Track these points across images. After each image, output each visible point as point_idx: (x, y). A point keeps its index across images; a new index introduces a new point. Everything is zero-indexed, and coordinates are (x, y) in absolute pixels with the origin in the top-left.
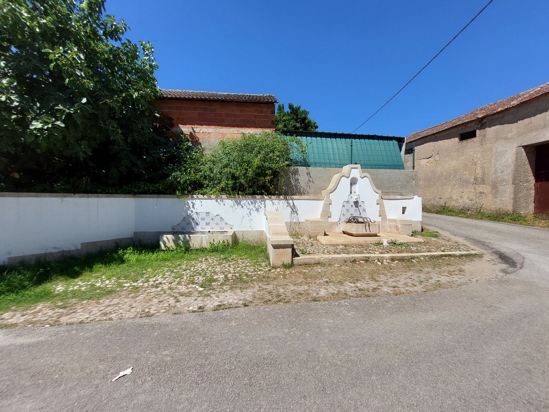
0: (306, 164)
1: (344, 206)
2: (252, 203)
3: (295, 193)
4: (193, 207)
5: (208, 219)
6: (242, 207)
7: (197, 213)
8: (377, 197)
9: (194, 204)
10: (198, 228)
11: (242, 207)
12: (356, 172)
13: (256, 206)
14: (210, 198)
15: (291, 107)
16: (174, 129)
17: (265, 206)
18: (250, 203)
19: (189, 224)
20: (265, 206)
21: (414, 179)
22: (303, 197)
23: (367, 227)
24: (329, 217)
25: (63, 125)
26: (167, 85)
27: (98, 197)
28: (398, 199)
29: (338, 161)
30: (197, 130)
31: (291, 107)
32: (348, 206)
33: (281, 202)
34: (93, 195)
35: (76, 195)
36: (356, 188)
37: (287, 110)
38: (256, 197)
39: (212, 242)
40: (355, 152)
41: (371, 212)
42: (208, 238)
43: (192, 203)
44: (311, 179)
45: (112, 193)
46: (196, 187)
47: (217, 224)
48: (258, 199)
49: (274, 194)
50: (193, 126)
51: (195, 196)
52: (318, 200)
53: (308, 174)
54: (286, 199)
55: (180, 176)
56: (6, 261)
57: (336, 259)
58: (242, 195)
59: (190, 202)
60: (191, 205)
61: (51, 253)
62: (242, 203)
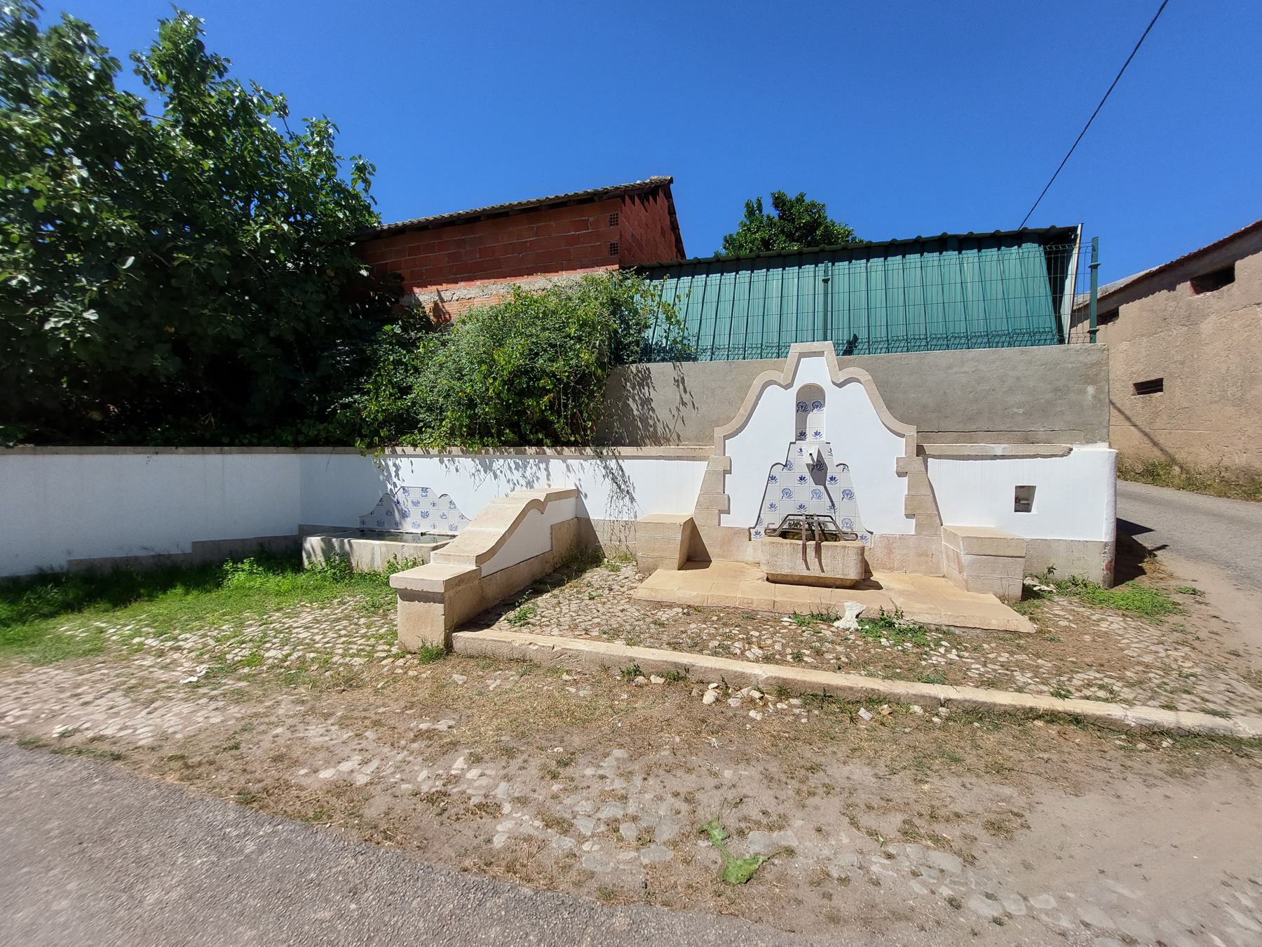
0: (679, 354)
1: (772, 478)
2: (517, 468)
3: (642, 438)
4: (397, 475)
5: (425, 505)
6: (496, 476)
7: (403, 488)
8: (900, 448)
9: (397, 468)
10: (407, 527)
11: (496, 476)
12: (817, 368)
13: (528, 474)
14: (427, 454)
15: (779, 202)
16: (405, 300)
17: (548, 475)
18: (513, 466)
19: (390, 513)
20: (548, 475)
21: (1093, 382)
22: (646, 450)
23: (811, 553)
24: (721, 512)
25: (47, 327)
26: (393, 207)
27: (222, 453)
28: (995, 457)
29: (900, 331)
30: (446, 296)
31: (779, 202)
32: (787, 479)
33: (586, 464)
34: (212, 449)
35: (181, 449)
36: (815, 419)
37: (770, 211)
38: (524, 453)
39: (392, 560)
40: (840, 301)
41: (875, 504)
42: (384, 549)
43: (395, 465)
44: (686, 398)
45: (251, 444)
46: (402, 427)
47: (443, 516)
48: (531, 456)
49: (568, 444)
50: (439, 287)
51: (399, 449)
52: (693, 459)
53: (680, 382)
54: (600, 456)
55: (372, 405)
56: (65, 565)
57: (575, 656)
58: (493, 445)
59: (390, 463)
60: (393, 469)
61: (136, 558)
62: (496, 465)
